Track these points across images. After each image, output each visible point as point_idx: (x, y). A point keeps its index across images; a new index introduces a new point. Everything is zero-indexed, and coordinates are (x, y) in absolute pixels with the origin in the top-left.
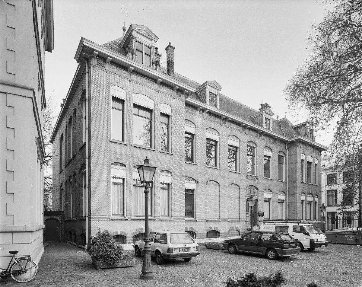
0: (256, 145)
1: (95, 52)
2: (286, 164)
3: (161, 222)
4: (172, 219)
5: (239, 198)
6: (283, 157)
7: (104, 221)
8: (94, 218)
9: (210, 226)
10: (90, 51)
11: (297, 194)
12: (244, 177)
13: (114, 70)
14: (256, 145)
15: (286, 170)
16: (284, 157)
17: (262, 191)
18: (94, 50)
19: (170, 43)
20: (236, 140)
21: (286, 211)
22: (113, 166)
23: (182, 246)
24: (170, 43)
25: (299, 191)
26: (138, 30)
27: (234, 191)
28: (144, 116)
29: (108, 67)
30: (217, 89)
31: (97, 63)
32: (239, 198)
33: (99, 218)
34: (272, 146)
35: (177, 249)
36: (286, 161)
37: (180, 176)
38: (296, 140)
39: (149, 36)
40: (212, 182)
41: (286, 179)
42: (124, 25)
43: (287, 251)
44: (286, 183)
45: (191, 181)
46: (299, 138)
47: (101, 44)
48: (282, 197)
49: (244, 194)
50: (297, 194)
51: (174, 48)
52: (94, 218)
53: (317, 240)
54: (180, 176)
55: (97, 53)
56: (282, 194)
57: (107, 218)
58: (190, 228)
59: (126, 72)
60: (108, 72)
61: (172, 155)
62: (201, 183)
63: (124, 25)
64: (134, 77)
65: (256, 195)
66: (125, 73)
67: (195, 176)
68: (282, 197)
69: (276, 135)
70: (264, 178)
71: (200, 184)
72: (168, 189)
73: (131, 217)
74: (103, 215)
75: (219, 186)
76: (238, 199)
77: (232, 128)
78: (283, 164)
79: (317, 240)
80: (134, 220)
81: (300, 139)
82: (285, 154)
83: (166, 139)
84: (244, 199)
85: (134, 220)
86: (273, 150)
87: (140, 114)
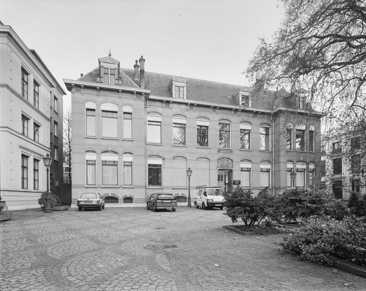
0: (231, 122)
1: (72, 85)
2: (272, 134)
3: (124, 189)
4: (163, 188)
5: (210, 169)
6: (269, 128)
7: (81, 188)
8: (73, 186)
9: (177, 193)
10: (70, 84)
11: (280, 162)
12: (216, 151)
13: (87, 92)
14: (231, 122)
15: (272, 140)
16: (270, 128)
17: (238, 162)
18: (71, 84)
19: (142, 57)
20: (206, 120)
21: (272, 179)
22: (86, 153)
23: (87, 200)
24: (142, 57)
25: (282, 159)
26: (104, 60)
27: (204, 164)
28: (111, 116)
29: (83, 91)
30: (184, 82)
31: (75, 90)
32: (210, 169)
33: (78, 187)
34: (251, 120)
35: (83, 201)
36: (272, 131)
37: (140, 156)
38: (277, 111)
39: (113, 63)
40: (179, 157)
41: (272, 148)
42: (110, 52)
43: (158, 205)
44: (272, 152)
45: (158, 158)
46: (279, 109)
47: (76, 79)
48: (268, 166)
49: (214, 166)
50: (280, 162)
51: (144, 60)
52: (73, 186)
53: (213, 200)
54: (140, 156)
55: (74, 85)
56: (266, 163)
57: (83, 186)
58: (181, 194)
59: (96, 91)
60: (83, 94)
61: (133, 141)
62: (167, 159)
63: (110, 52)
64: (102, 93)
65: (231, 166)
66: (95, 92)
67: (161, 154)
68: (268, 166)
69: (254, 110)
70: (240, 150)
71: (166, 160)
72: (131, 166)
73: (100, 186)
74: (80, 185)
75: (186, 160)
76: (209, 170)
77: (202, 111)
78: (269, 135)
79: (212, 200)
80: (102, 188)
81: (280, 110)
82: (270, 126)
83: (358, 91)
84: (215, 169)
85: (102, 188)
86: (252, 124)
87: (113, 117)
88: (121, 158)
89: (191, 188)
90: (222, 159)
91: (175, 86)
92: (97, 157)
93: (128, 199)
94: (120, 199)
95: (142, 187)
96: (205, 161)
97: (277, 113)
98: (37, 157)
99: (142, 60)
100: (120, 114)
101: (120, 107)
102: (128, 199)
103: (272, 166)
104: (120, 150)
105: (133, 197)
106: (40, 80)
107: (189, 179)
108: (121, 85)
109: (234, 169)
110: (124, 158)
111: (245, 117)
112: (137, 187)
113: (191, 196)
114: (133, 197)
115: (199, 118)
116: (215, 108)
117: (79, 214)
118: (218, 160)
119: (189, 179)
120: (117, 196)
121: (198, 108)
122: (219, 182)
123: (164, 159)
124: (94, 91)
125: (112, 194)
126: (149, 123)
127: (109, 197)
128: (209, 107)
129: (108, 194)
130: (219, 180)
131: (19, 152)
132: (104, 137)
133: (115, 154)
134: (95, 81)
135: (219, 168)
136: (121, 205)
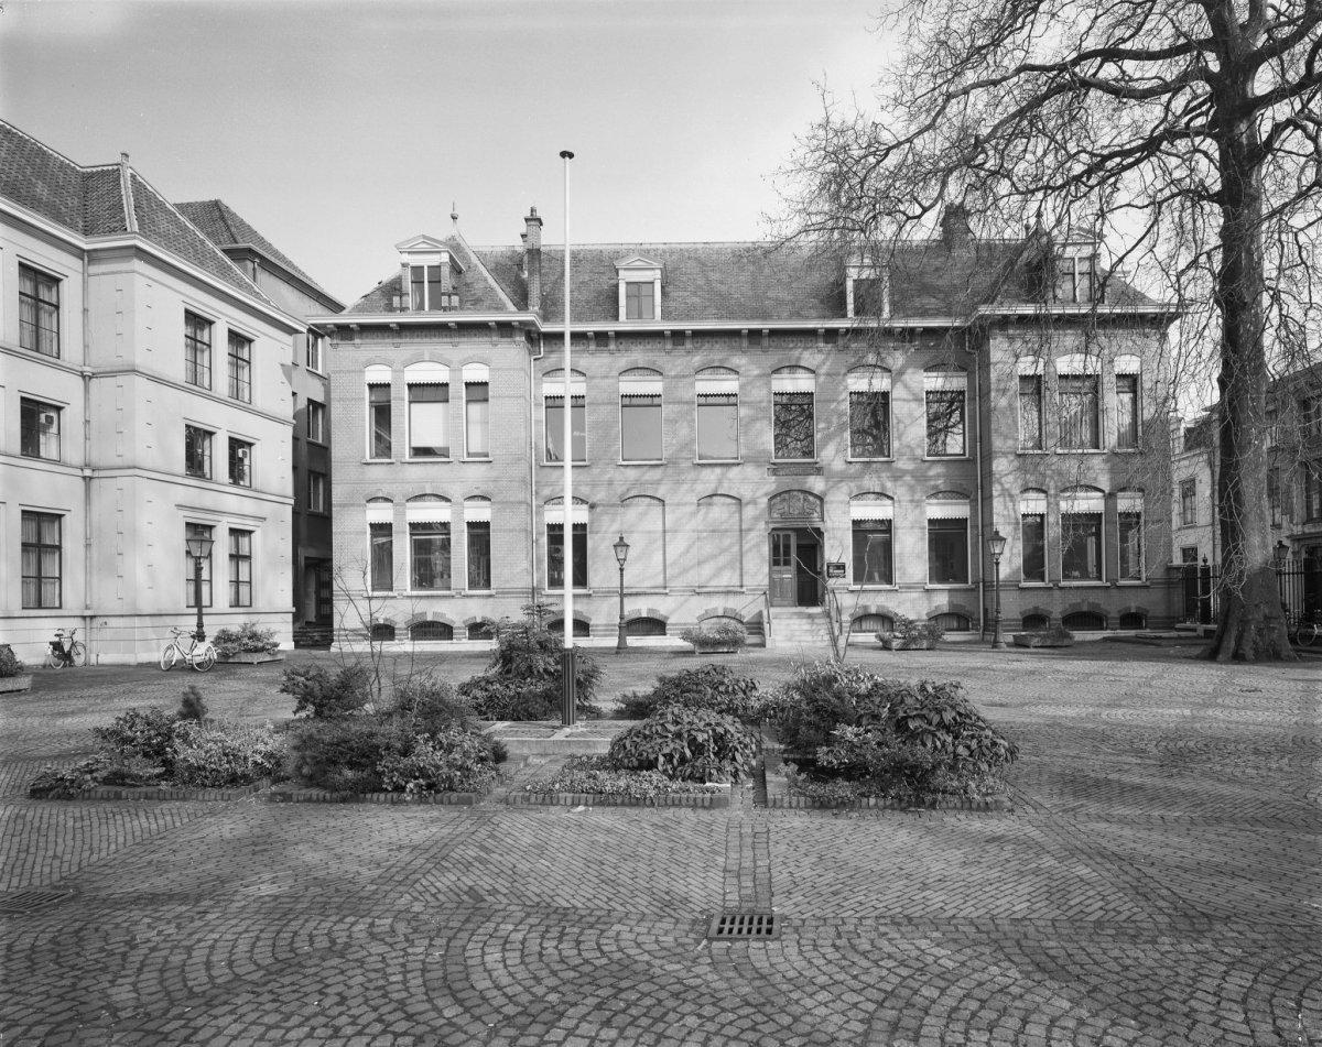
3: (467, 600)
34: (738, 360)
88: (400, 514)
90: (786, 496)
92: (395, 514)
96: (723, 504)
98: (239, 524)
99: (534, 220)
100: (458, 392)
101: (456, 371)
103: (1146, 502)
104: (456, 492)
105: (667, 618)
106: (247, 324)
107: (622, 570)
108: (455, 308)
109: (829, 524)
110: (408, 513)
111: (638, 354)
113: (204, 629)
115: (706, 372)
116: (755, 335)
119: (622, 570)
121: (776, 341)
122: (776, 568)
123: (592, 507)
125: (650, 610)
126: (703, 400)
129: (639, 610)
130: (776, 563)
131: (181, 518)
132: (964, 448)
133: (443, 503)
134: (390, 308)
135: (772, 526)
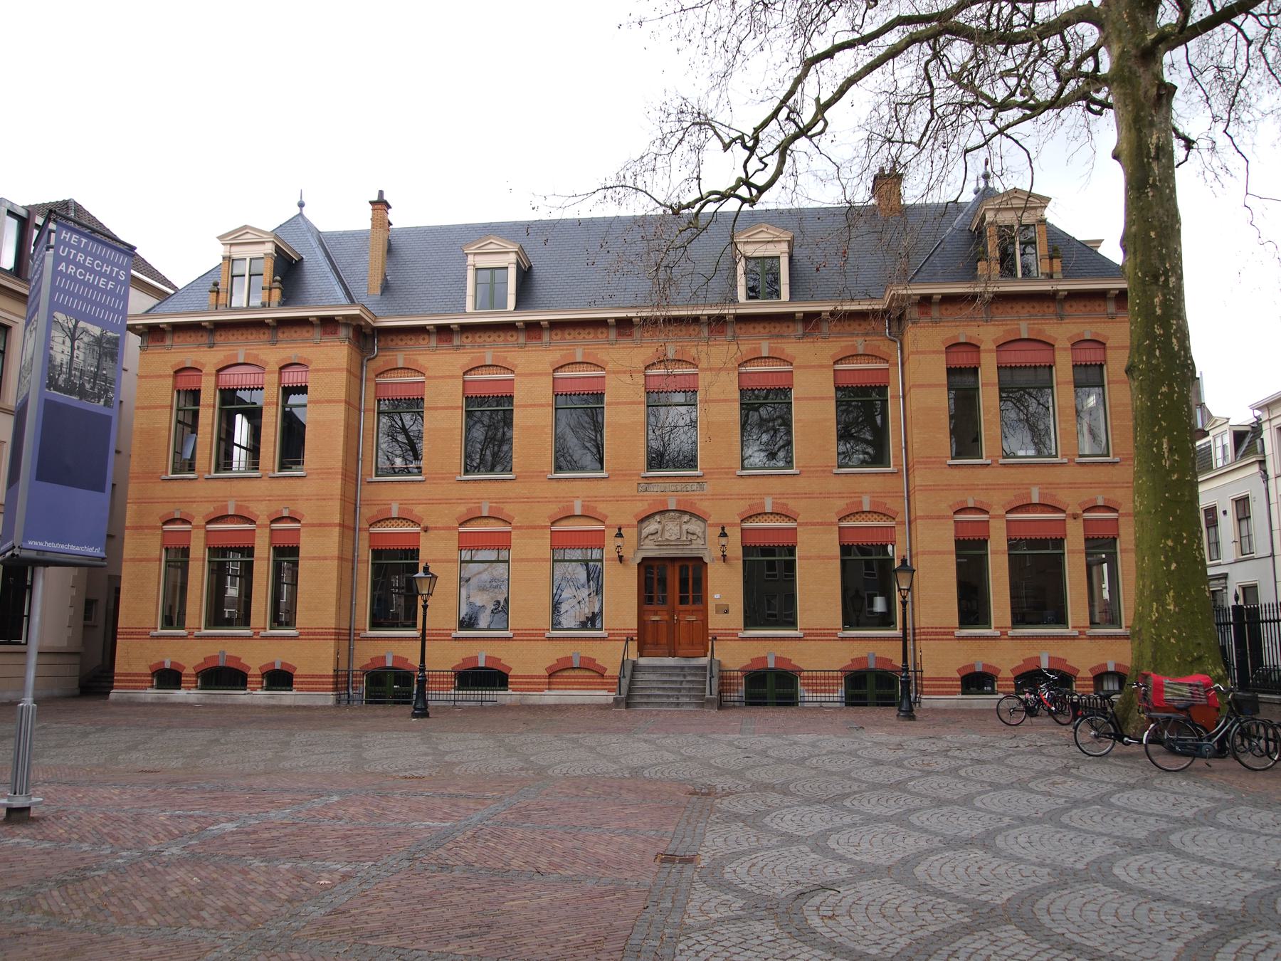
19: (381, 193)
24: (381, 193)
38: (343, 316)
64: (219, 338)
89: (921, 634)
91: (477, 269)
93: (279, 678)
94: (187, 675)
95: (326, 634)
97: (163, 330)
102: (279, 678)
105: (295, 669)
112: (308, 634)
114: (295, 669)
117: (803, 738)
118: (642, 521)
120: (243, 665)
121: (557, 336)
124: (304, 331)
127: (976, 673)
128: (601, 324)
136: (258, 696)
